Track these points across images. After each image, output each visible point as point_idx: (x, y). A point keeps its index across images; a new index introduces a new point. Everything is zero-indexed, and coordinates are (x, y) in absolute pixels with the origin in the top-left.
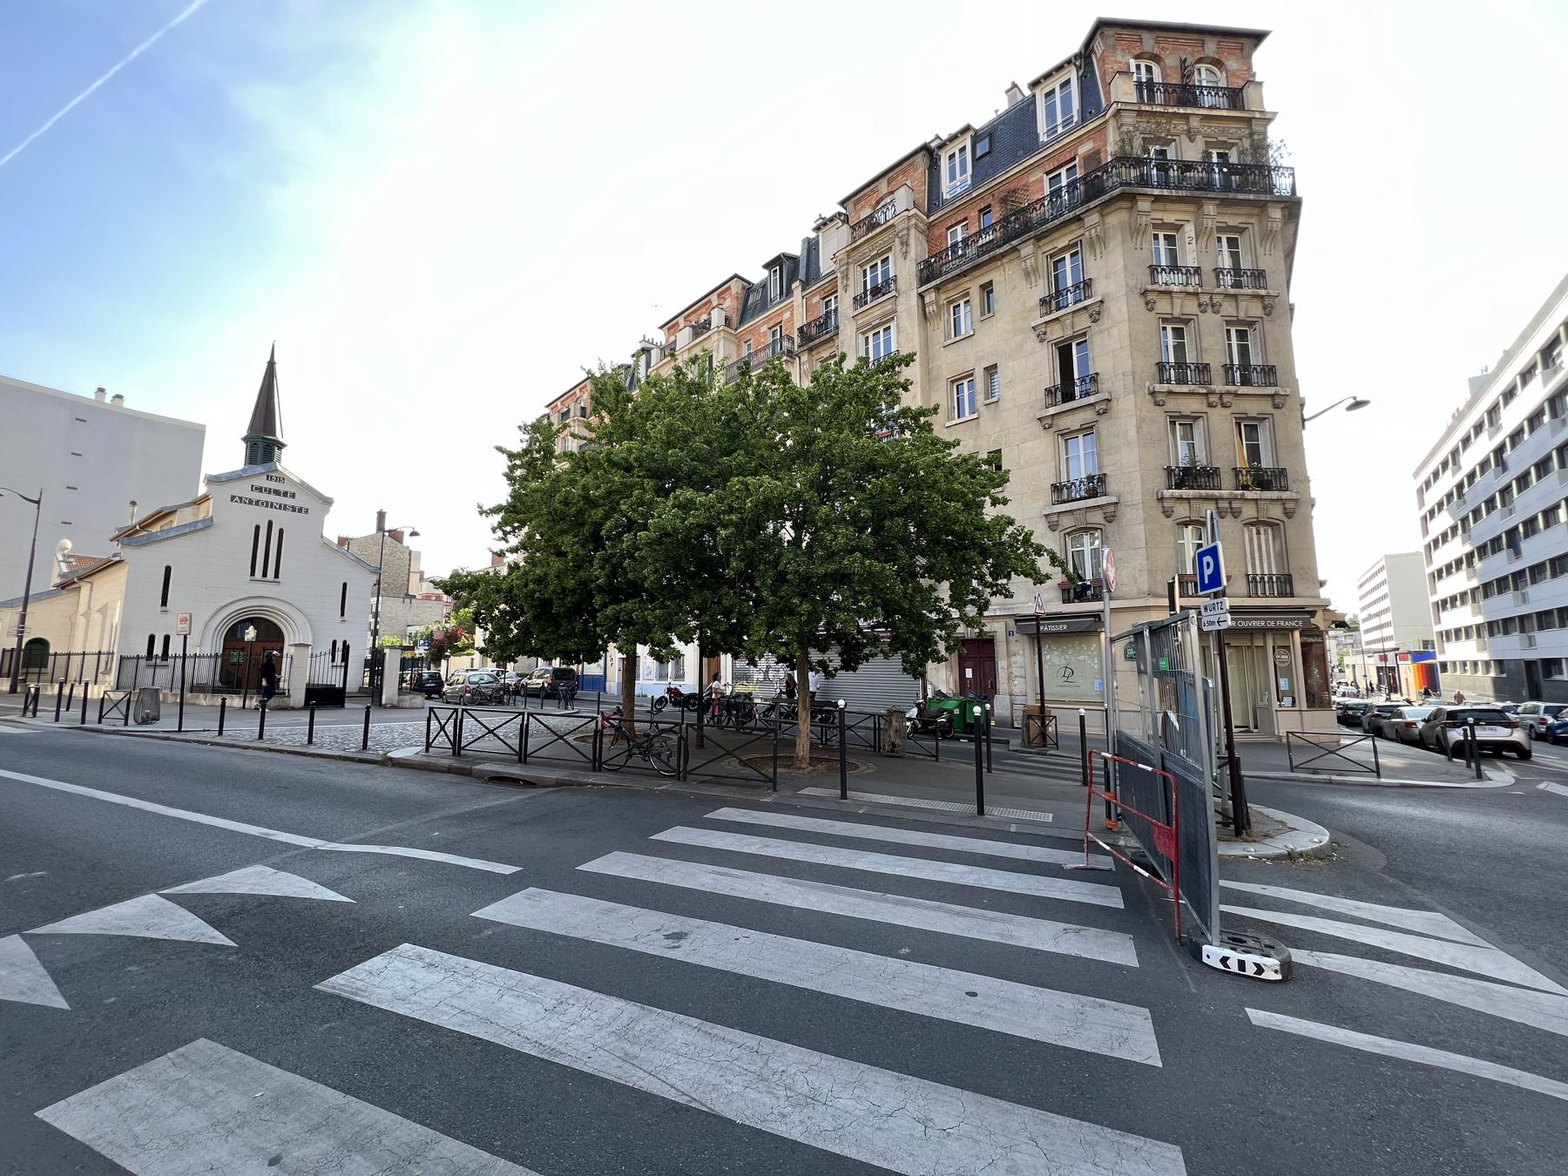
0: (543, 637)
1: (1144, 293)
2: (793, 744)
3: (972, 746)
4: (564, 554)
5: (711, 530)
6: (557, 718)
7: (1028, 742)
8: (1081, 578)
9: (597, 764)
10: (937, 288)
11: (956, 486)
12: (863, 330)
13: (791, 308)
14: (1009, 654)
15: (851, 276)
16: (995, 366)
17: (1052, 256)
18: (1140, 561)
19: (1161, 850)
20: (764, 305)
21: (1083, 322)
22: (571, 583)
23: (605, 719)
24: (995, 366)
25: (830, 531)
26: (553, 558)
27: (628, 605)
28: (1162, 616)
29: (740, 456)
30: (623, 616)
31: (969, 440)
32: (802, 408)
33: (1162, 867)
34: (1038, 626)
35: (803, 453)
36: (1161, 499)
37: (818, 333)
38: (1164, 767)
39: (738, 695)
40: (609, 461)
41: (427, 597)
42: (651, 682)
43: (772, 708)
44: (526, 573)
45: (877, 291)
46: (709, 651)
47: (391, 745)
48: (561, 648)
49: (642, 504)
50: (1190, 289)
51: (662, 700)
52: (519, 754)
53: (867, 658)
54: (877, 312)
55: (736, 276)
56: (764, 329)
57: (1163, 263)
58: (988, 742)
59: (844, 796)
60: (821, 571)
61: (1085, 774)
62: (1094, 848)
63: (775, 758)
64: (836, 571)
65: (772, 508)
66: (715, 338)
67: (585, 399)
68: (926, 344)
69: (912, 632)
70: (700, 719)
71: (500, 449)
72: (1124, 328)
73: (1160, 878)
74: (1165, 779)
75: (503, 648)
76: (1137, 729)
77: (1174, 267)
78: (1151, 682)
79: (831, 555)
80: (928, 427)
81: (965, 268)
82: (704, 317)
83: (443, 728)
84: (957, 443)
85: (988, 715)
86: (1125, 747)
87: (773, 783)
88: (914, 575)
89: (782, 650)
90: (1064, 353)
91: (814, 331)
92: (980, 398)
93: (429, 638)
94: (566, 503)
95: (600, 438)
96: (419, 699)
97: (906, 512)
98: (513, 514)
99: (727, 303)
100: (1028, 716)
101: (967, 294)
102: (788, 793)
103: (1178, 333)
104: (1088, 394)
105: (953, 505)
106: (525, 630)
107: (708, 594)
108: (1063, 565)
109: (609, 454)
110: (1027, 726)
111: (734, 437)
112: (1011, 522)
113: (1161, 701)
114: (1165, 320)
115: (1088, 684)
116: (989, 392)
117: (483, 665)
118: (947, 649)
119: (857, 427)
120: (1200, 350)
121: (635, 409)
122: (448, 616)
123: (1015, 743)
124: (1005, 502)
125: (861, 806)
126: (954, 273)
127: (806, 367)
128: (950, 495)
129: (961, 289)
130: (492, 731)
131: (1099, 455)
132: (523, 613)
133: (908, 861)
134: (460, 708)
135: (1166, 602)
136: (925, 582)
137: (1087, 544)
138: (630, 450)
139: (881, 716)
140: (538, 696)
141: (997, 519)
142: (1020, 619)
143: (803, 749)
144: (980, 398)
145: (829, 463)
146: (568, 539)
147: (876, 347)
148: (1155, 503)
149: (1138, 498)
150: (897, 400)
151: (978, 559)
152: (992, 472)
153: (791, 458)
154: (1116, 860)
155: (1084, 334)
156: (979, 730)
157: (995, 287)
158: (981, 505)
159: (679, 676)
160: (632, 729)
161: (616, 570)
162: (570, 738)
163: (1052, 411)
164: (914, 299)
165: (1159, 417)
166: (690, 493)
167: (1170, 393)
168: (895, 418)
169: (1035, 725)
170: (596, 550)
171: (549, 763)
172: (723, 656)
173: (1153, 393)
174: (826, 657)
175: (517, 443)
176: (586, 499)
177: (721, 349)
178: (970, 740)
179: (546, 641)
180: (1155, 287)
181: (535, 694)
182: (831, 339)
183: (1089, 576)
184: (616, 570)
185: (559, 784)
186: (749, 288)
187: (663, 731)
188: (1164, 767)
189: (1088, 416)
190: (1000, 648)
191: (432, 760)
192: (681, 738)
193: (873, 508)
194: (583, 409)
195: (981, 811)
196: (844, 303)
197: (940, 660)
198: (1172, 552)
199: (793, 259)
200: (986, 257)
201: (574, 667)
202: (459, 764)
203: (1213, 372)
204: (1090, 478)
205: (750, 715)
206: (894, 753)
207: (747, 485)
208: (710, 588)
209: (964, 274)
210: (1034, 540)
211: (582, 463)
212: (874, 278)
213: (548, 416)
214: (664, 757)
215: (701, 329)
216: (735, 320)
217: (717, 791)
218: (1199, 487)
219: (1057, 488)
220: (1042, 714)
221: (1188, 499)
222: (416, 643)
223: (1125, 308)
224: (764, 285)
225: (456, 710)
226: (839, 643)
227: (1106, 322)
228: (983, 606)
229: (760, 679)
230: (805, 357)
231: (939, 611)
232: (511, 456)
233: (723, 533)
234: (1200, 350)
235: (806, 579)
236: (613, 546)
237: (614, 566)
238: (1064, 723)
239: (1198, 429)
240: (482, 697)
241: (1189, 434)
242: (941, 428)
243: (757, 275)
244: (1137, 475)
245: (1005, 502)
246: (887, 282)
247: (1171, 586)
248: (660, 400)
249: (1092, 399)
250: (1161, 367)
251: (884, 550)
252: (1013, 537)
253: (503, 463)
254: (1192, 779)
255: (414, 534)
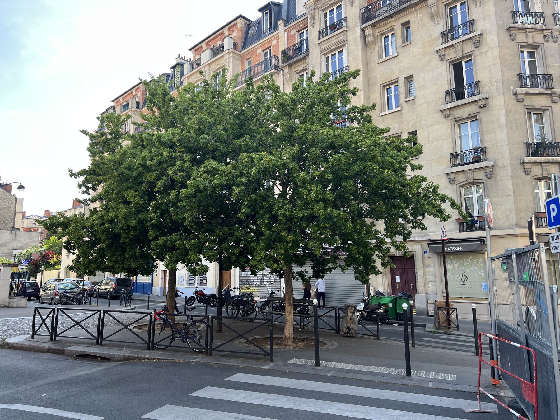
0: (114, 259)
1: (509, 29)
2: (282, 329)
3: (402, 329)
4: (129, 203)
5: (228, 187)
6: (122, 314)
7: (438, 326)
8: (470, 215)
9: (151, 345)
10: (373, 26)
11: (389, 159)
12: (325, 53)
13: (277, 38)
14: (424, 266)
15: (317, 17)
16: (412, 76)
17: (448, 5)
18: (510, 204)
19: (527, 399)
20: (259, 35)
21: (469, 48)
22: (133, 223)
23: (157, 314)
24: (412, 76)
25: (306, 188)
26: (121, 205)
27: (173, 237)
28: (522, 243)
29: (247, 139)
30: (169, 244)
31: (392, 123)
32: (286, 109)
33: (528, 410)
34: (443, 247)
35: (289, 136)
36: (523, 163)
37: (295, 54)
38: (528, 345)
39: (244, 295)
40: (159, 141)
41: (27, 230)
42: (185, 286)
43: (267, 303)
44: (102, 216)
45: (334, 27)
46: (225, 267)
47: (7, 334)
48: (126, 266)
49: (182, 170)
50: (538, 27)
51: (192, 299)
52: (97, 339)
53: (330, 270)
54: (334, 41)
55: (241, 16)
56: (259, 51)
57: (520, 10)
58: (413, 326)
59: (318, 364)
60: (300, 214)
61: (477, 347)
62: (484, 398)
63: (271, 339)
64: (310, 215)
65: (268, 173)
66: (227, 57)
67: (139, 96)
68: (366, 62)
69: (360, 253)
70: (220, 312)
71: (84, 132)
72: (496, 52)
73: (527, 417)
74: (528, 352)
75: (86, 266)
76: (510, 318)
77: (527, 13)
78: (518, 288)
79: (307, 204)
80: (368, 120)
81: (391, 12)
82: (219, 43)
83: (44, 322)
84: (388, 130)
85: (411, 307)
86: (502, 331)
87: (270, 356)
88: (361, 216)
89: (275, 266)
90: (457, 67)
91: (292, 53)
92: (402, 97)
93: (29, 259)
94: (129, 168)
95: (153, 126)
96: (23, 301)
97: (354, 177)
98: (92, 176)
99: (235, 34)
100: (438, 308)
101: (393, 29)
102: (280, 363)
103: (532, 55)
104: (473, 94)
105: (387, 172)
106: (102, 254)
107: (226, 229)
108: (459, 208)
109: (159, 136)
110: (438, 315)
111: (242, 125)
112: (424, 180)
113: (527, 297)
114: (522, 47)
115: (477, 287)
116: (408, 93)
117: (67, 276)
118: (383, 265)
119: (322, 121)
120: (545, 66)
121: (176, 107)
122: (42, 243)
123: (430, 326)
124: (420, 168)
125: (329, 371)
126: (384, 16)
127: (287, 76)
128: (384, 165)
129: (389, 26)
130: (78, 323)
131: (481, 135)
132: (99, 241)
133: (362, 408)
134: (56, 307)
135: (526, 231)
136: (368, 221)
137: (475, 193)
138: (174, 135)
139: (340, 309)
140: (105, 298)
141: (414, 178)
142: (431, 243)
143: (289, 331)
144: (402, 97)
145: (305, 144)
146: (131, 193)
147: (334, 64)
148: (519, 166)
149: (507, 162)
150: (348, 101)
151: (403, 205)
152: (411, 146)
153: (281, 139)
154: (499, 406)
155: (470, 55)
156: (406, 319)
157: (412, 25)
158: (404, 170)
159: (203, 282)
160: (173, 320)
161: (165, 213)
162: (131, 327)
163: (450, 105)
164: (358, 32)
165: (520, 109)
166: (214, 164)
167: (527, 93)
168: (347, 113)
169: (443, 314)
170: (150, 200)
171: (119, 344)
172: (233, 270)
173: (516, 94)
174: (303, 269)
175: (93, 127)
176: (144, 166)
177: (231, 65)
178: (400, 325)
179: (116, 262)
180: (516, 25)
181: (102, 296)
182: (304, 58)
183: (476, 214)
184: (165, 213)
185: (125, 359)
186: (249, 24)
187: (196, 321)
188: (528, 345)
189: (474, 109)
190: (418, 262)
191: (37, 344)
192: (208, 326)
193: (333, 173)
194: (138, 103)
195: (409, 374)
196: (313, 34)
197: (377, 273)
198: (531, 198)
199: (278, 5)
200: (405, 6)
201: (131, 278)
202: (57, 346)
203: (554, 80)
204: (476, 150)
205: (252, 309)
206: (349, 335)
207: (252, 159)
208: (228, 226)
209: (391, 16)
210: (440, 191)
211: (140, 142)
212: (332, 19)
213: (113, 108)
214: (196, 339)
215: (217, 51)
216: (240, 45)
217: (232, 362)
218: (548, 155)
219: (454, 156)
220: (447, 307)
221: (541, 163)
222: (19, 261)
223: (496, 39)
224: (259, 22)
225: (53, 309)
226: (311, 260)
227: (484, 48)
228: (406, 236)
229: (260, 284)
230: (286, 70)
231: (378, 239)
232: (92, 137)
233: (237, 190)
234: (545, 66)
235: (290, 219)
236: (162, 198)
237: (163, 211)
238: (463, 313)
239: (546, 116)
240: (77, 298)
241: (540, 120)
242: (379, 122)
243: (254, 16)
244: (506, 148)
245: (420, 168)
246: (340, 21)
247: (530, 223)
248: (194, 103)
249: (476, 98)
250: (521, 77)
251: (341, 200)
252: (427, 189)
253: (86, 141)
254: (546, 352)
255: (21, 187)
